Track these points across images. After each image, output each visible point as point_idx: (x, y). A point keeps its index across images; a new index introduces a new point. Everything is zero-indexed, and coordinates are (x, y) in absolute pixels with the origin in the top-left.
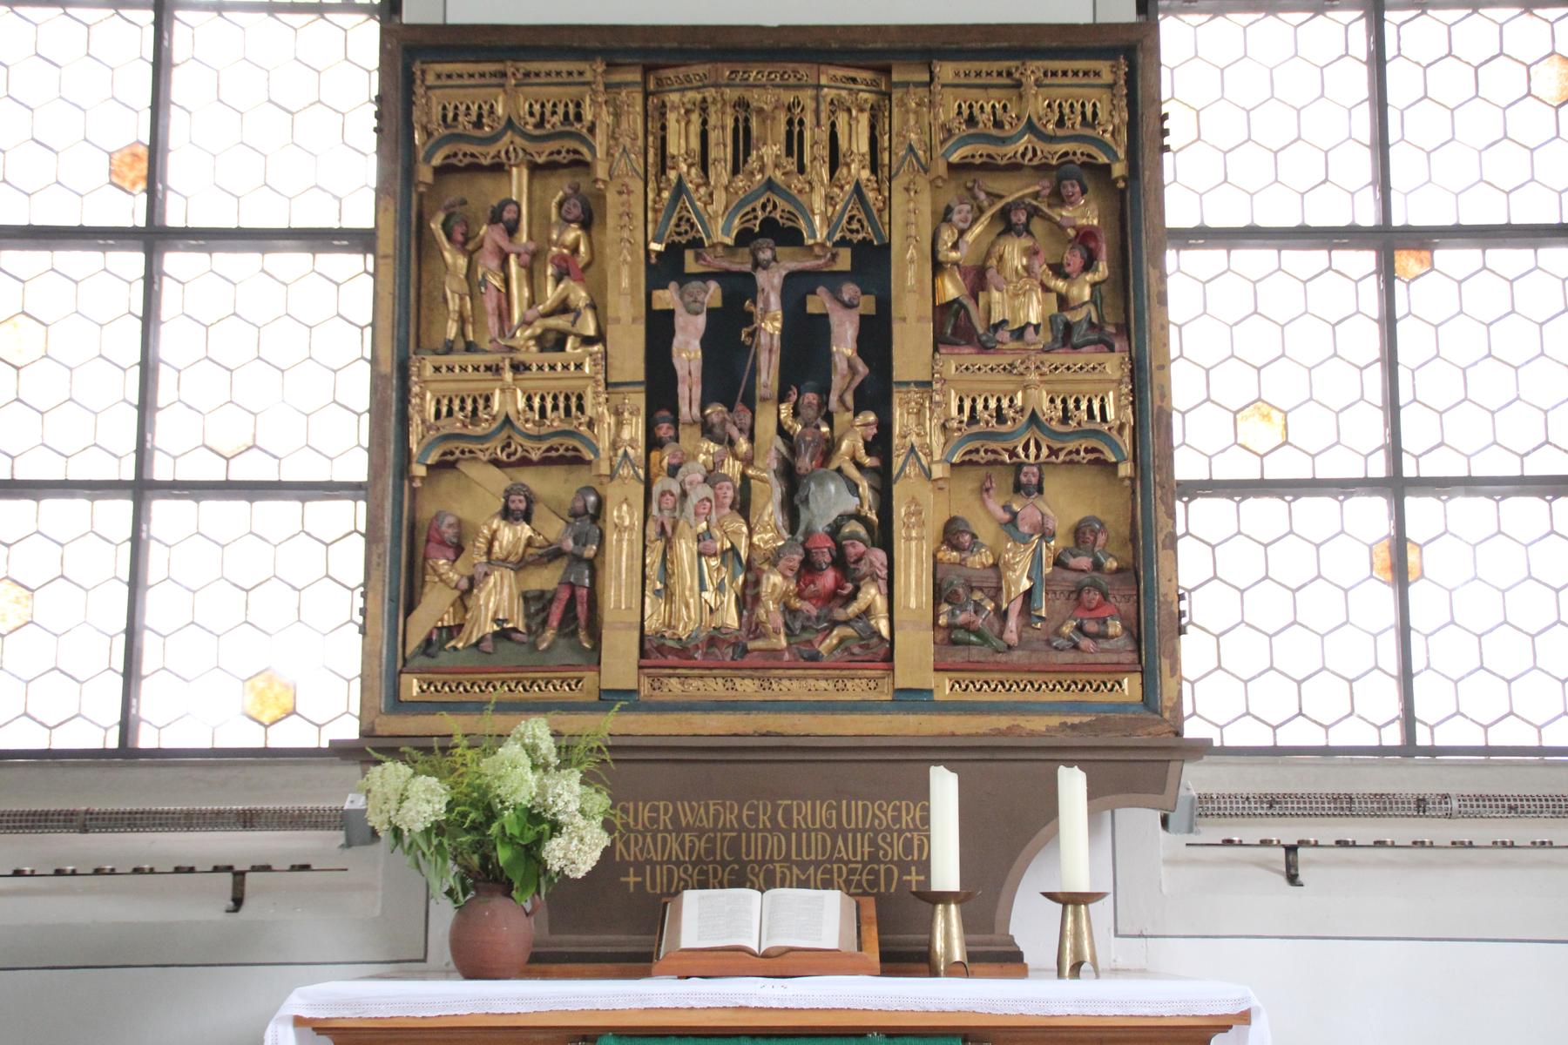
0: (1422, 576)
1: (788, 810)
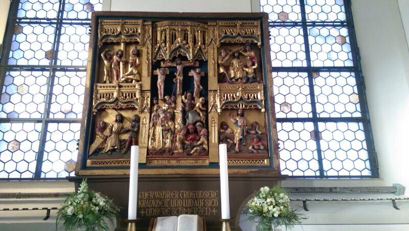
0: (322, 139)
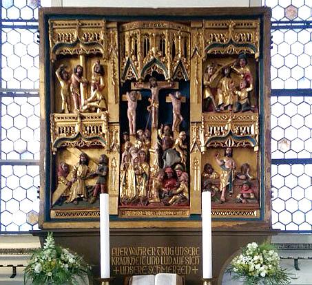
1: (160, 250)
